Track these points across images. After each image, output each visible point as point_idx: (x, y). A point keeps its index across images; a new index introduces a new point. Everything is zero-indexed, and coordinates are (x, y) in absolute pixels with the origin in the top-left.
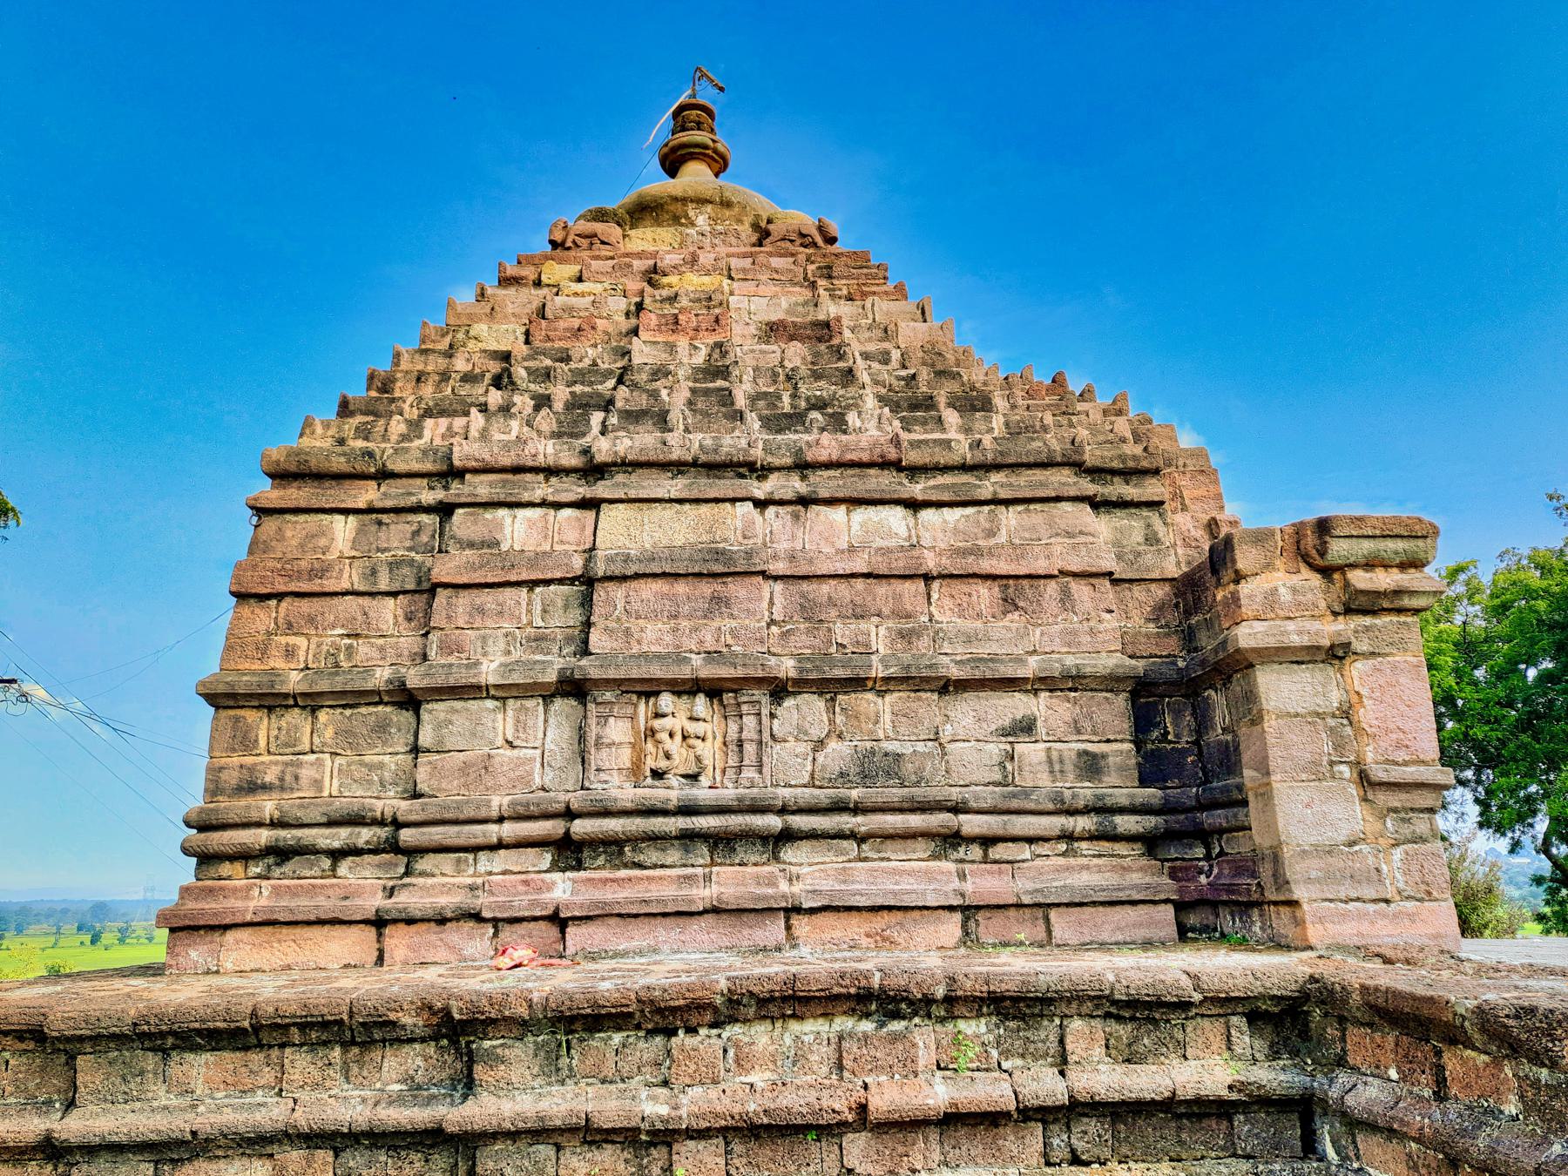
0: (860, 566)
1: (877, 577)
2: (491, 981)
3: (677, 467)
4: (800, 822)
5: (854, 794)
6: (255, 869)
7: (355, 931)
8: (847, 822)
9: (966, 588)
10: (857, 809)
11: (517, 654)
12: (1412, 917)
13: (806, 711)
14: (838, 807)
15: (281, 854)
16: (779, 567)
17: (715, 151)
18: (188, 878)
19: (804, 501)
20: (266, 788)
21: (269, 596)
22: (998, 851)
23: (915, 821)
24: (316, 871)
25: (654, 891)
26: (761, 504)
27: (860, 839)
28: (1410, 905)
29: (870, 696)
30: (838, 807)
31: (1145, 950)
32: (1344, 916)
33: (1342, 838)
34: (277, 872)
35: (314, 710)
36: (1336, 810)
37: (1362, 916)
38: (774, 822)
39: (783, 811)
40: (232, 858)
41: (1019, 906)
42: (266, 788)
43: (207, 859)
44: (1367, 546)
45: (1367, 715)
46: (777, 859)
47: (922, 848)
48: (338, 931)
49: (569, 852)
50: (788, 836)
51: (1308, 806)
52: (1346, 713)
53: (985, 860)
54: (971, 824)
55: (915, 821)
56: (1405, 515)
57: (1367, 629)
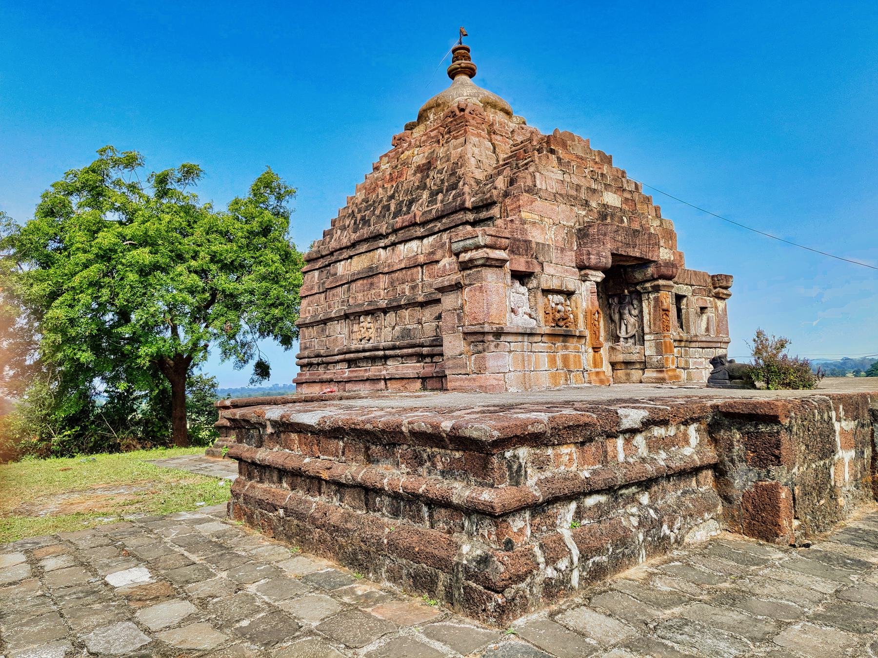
0: (403, 266)
1: (408, 268)
3: (366, 240)
4: (388, 353)
5: (398, 343)
8: (398, 352)
9: (431, 267)
10: (400, 348)
12: (474, 380)
13: (391, 317)
14: (394, 348)
16: (386, 270)
17: (461, 68)
18: (299, 371)
22: (435, 359)
23: (410, 351)
25: (362, 374)
26: (385, 248)
27: (402, 356)
28: (474, 375)
29: (404, 310)
32: (457, 380)
33: (458, 353)
36: (457, 343)
37: (461, 379)
38: (381, 353)
39: (384, 349)
41: (433, 377)
43: (302, 366)
44: (462, 244)
45: (466, 308)
46: (386, 364)
47: (414, 360)
50: (386, 358)
51: (450, 342)
52: (462, 308)
53: (432, 362)
54: (425, 350)
55: (410, 351)
57: (469, 275)
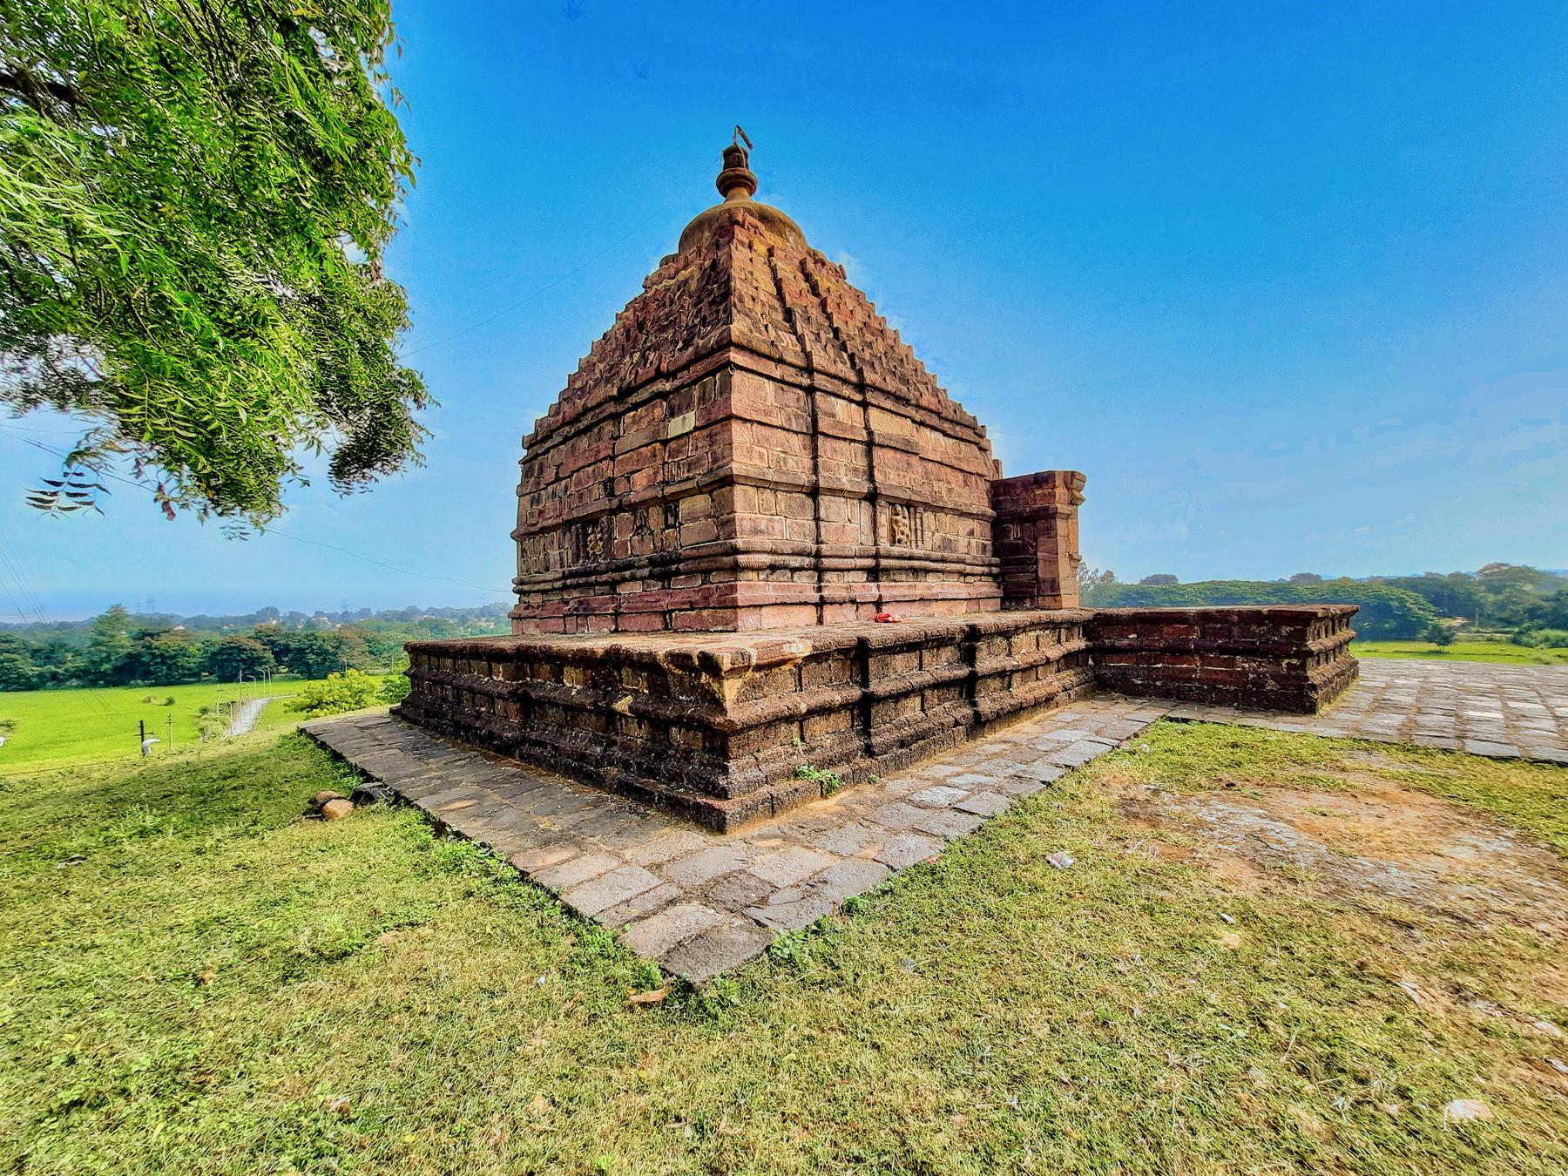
2: (76, 784)
6: (762, 576)
7: (809, 607)
11: (169, 368)
15: (773, 568)
19: (922, 424)
20: (761, 532)
21: (750, 421)
22: (969, 579)
24: (785, 579)
30: (943, 560)
31: (197, 822)
34: (771, 578)
35: (776, 491)
40: (753, 569)
42: (761, 532)
48: (803, 608)
49: (874, 573)
50: (927, 571)
56: (609, 324)
